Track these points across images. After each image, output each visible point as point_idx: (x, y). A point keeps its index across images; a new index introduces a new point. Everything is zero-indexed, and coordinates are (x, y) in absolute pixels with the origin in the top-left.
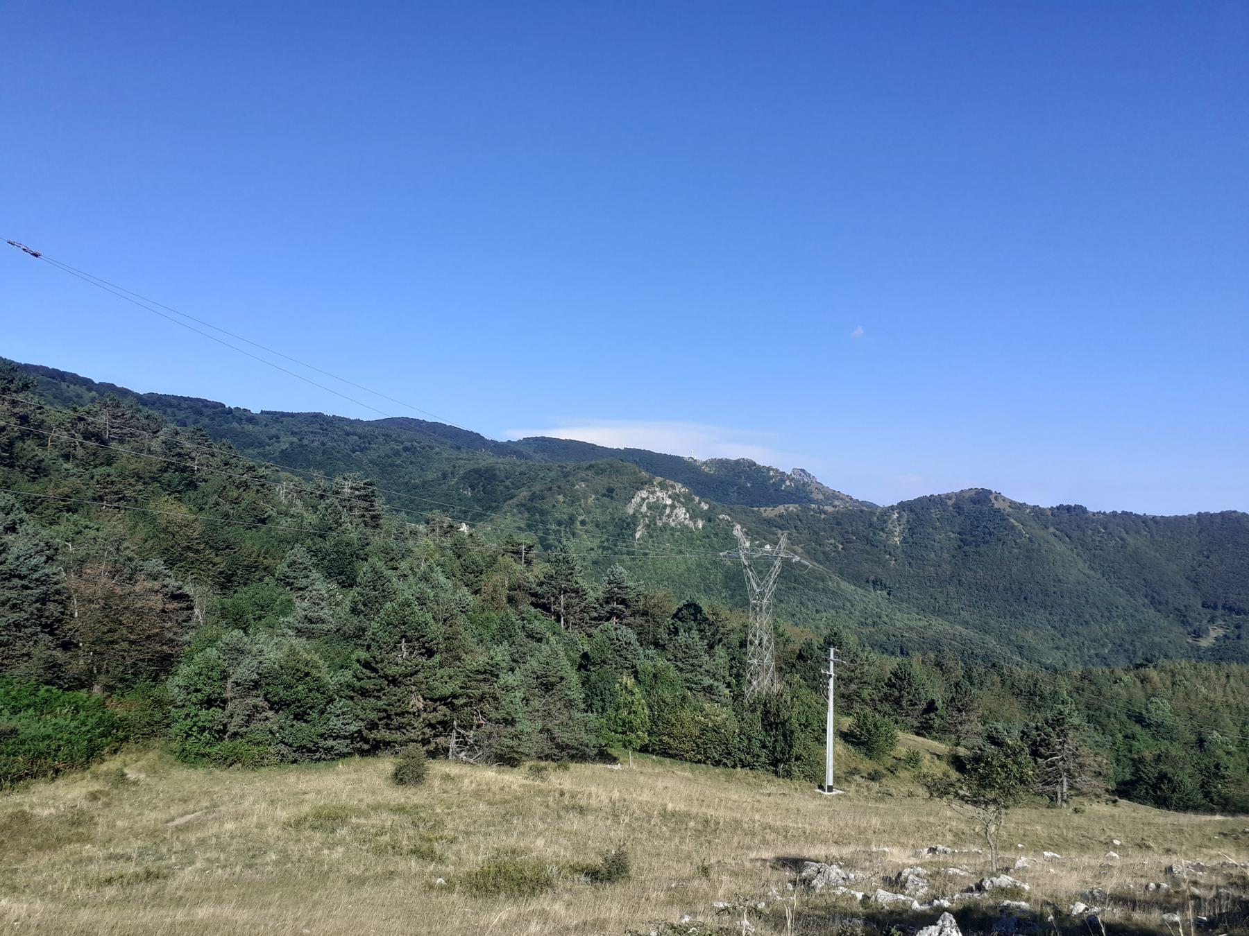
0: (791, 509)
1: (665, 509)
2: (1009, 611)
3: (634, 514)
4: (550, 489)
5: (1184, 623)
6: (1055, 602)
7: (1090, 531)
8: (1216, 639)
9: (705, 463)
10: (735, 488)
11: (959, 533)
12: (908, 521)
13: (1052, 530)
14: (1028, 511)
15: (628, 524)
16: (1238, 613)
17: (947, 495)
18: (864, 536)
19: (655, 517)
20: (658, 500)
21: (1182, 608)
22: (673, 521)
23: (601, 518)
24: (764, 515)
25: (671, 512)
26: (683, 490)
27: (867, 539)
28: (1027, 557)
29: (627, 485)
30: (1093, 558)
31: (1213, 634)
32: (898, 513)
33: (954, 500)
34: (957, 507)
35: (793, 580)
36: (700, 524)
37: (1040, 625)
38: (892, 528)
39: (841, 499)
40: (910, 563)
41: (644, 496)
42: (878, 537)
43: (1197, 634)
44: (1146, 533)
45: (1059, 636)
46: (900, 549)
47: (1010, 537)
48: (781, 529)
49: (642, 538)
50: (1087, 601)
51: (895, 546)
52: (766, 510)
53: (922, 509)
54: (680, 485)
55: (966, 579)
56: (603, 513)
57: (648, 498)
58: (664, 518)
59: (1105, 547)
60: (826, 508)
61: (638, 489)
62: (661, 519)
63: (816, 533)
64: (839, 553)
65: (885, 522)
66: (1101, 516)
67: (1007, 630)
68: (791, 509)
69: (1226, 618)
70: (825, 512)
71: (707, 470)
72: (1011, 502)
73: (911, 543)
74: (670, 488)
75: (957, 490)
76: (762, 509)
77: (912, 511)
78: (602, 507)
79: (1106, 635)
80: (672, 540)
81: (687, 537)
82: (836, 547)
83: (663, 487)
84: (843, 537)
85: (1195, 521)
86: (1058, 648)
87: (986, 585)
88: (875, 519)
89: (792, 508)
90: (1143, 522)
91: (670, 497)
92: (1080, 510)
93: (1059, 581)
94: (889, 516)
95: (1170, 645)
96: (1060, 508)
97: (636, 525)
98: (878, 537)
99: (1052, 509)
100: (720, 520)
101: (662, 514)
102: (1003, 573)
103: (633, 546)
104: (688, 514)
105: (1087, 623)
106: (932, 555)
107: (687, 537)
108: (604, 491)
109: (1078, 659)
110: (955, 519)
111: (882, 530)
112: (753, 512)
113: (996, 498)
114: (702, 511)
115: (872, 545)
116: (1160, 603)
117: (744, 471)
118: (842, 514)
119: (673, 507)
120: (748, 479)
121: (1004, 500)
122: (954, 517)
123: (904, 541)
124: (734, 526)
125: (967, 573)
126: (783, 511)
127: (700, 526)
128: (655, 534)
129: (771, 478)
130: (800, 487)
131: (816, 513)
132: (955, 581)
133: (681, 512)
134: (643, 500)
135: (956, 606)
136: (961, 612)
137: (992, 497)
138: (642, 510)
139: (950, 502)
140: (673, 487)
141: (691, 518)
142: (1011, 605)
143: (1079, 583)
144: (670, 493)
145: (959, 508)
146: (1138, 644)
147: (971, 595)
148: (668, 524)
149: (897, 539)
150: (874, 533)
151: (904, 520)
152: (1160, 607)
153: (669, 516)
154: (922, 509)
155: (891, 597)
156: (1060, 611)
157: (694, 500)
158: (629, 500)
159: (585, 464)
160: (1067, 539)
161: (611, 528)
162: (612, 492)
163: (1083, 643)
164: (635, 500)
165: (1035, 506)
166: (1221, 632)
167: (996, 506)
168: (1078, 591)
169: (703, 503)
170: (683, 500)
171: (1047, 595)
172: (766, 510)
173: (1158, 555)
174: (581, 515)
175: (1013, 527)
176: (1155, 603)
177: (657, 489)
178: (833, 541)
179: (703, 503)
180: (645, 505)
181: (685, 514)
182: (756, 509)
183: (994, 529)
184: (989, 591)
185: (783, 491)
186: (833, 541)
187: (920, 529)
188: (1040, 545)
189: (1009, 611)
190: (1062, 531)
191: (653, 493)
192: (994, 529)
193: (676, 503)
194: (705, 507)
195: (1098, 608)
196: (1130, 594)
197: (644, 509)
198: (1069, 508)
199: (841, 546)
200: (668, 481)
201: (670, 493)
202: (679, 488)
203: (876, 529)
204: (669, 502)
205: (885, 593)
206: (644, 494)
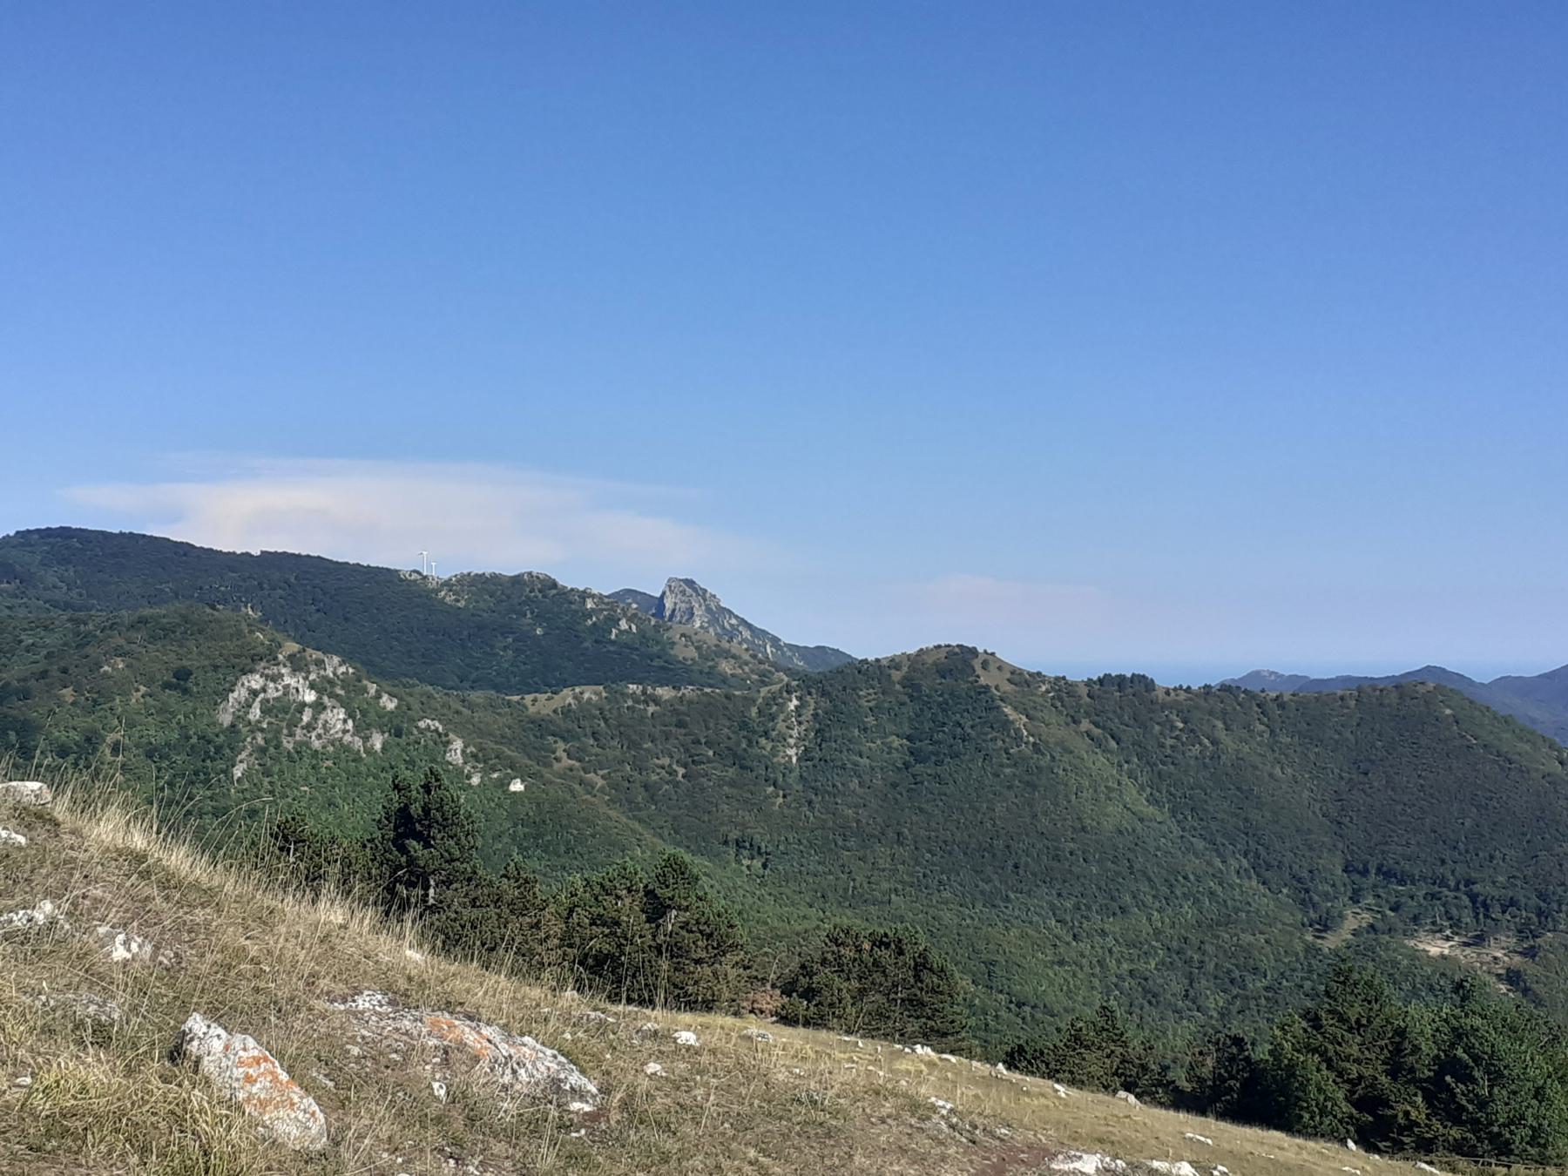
0: (586, 696)
1: (301, 713)
2: (982, 893)
3: (233, 726)
4: (44, 674)
5: (1305, 903)
6: (1070, 872)
7: (1157, 728)
8: (1355, 933)
9: (447, 584)
10: (510, 640)
11: (909, 738)
12: (815, 716)
13: (1085, 725)
14: (1044, 688)
15: (218, 749)
16: (1401, 882)
17: (892, 660)
18: (729, 749)
19: (279, 731)
20: (285, 694)
21: (1305, 874)
22: (319, 737)
23: (156, 736)
24: (532, 710)
25: (315, 719)
26: (343, 669)
27: (735, 755)
28: (1028, 784)
29: (220, 661)
30: (1156, 780)
31: (1351, 923)
32: (798, 698)
33: (905, 669)
34: (909, 683)
35: (562, 849)
36: (377, 742)
37: (1036, 918)
38: (784, 730)
39: (734, 657)
40: (810, 803)
41: (255, 686)
42: (756, 751)
43: (1324, 925)
44: (1262, 728)
45: (1069, 938)
46: (796, 773)
47: (1000, 743)
48: (564, 739)
49: (247, 775)
50: (1131, 867)
51: (788, 768)
52: (535, 700)
53: (844, 689)
54: (336, 659)
55: (910, 830)
56: (163, 725)
57: (264, 690)
58: (298, 731)
59: (1180, 757)
60: (659, 691)
61: (245, 672)
62: (291, 735)
63: (634, 745)
64: (676, 785)
65: (773, 718)
66: (1183, 696)
67: (971, 930)
68: (586, 696)
69: (1381, 891)
70: (656, 701)
71: (450, 599)
72: (1015, 672)
73: (816, 761)
74: (312, 668)
75: (912, 650)
76: (529, 698)
77: (824, 694)
78: (160, 711)
79: (1157, 933)
80: (312, 780)
81: (347, 771)
82: (672, 773)
83: (297, 665)
84: (687, 750)
85: (1353, 703)
86: (1061, 963)
87: (945, 842)
88: (754, 711)
89: (589, 693)
90: (1258, 705)
91: (312, 686)
92: (1142, 683)
93: (1083, 829)
94: (782, 706)
95: (1268, 949)
96: (1104, 681)
97: (235, 751)
98: (756, 751)
99: (1089, 683)
100: (421, 731)
101: (293, 724)
102: (979, 816)
103: (226, 795)
104: (350, 722)
105: (1123, 910)
106: (854, 784)
107: (347, 771)
108: (169, 677)
109: (1096, 982)
110: (904, 709)
111: (766, 734)
112: (509, 704)
113: (985, 665)
114: (382, 713)
115: (742, 767)
116: (1269, 867)
117: (529, 602)
118: (690, 702)
119: (318, 707)
120: (539, 618)
121: (999, 668)
122: (903, 704)
123: (805, 757)
124: (449, 742)
125: (914, 818)
126: (570, 700)
127: (378, 746)
128: (276, 769)
129: (589, 614)
130: (650, 634)
131: (638, 703)
132: (891, 834)
133: (336, 718)
134: (254, 693)
135: (885, 886)
136: (893, 896)
137: (977, 664)
138: (251, 717)
139: (896, 675)
140: (320, 664)
141: (358, 730)
142: (988, 881)
143: (1121, 832)
144: (312, 677)
145: (912, 686)
146: (1209, 949)
147: (917, 863)
148: (307, 744)
149: (792, 752)
150: (750, 741)
151: (808, 714)
152: (1268, 875)
153: (310, 727)
154: (844, 689)
155: (768, 872)
156: (1078, 889)
157: (365, 690)
158: (224, 694)
159: (126, 615)
160: (1113, 744)
161: (179, 758)
162: (186, 680)
163: (1110, 951)
164: (235, 694)
165: (1057, 679)
166: (1367, 918)
167: (982, 681)
168: (1116, 849)
169: (385, 697)
170: (342, 692)
171: (1057, 858)
172: (535, 700)
173: (1277, 771)
174: (112, 730)
175: (1006, 724)
176: (1260, 867)
177: (284, 671)
178: (666, 761)
179: (385, 697)
180: (257, 704)
181: (345, 721)
182: (516, 698)
183: (972, 727)
184: (950, 853)
185: (613, 643)
186: (666, 761)
187: (836, 732)
188: (1053, 758)
189: (982, 893)
190: (1104, 728)
191: (275, 678)
192: (972, 727)
193: (325, 699)
194: (390, 704)
195: (1150, 880)
196: (1217, 850)
197: (255, 713)
198: (1120, 681)
199: (681, 771)
200: (309, 651)
201: (312, 677)
202: (334, 666)
203: (754, 732)
204: (310, 697)
205: (757, 863)
206: (256, 682)
